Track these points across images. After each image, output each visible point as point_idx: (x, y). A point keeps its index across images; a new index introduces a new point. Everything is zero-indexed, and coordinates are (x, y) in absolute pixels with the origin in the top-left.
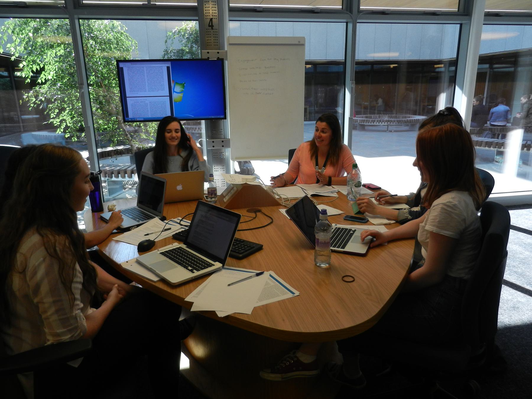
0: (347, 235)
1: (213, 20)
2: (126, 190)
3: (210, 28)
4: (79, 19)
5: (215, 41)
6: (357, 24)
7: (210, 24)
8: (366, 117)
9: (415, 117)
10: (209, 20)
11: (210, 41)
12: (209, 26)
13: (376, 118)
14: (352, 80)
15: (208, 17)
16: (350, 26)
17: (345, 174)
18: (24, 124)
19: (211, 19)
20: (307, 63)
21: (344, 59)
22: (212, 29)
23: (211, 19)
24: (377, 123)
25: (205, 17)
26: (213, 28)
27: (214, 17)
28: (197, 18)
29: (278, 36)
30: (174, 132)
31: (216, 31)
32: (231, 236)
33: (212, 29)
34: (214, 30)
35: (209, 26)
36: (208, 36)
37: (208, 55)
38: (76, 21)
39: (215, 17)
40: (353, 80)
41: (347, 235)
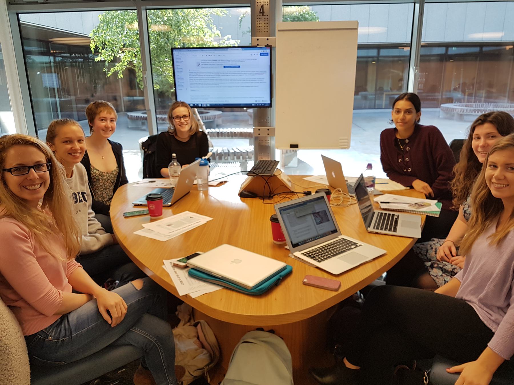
0: (384, 219)
1: (264, 6)
2: (164, 199)
3: (261, 14)
4: (146, 9)
5: (265, 28)
6: (425, 4)
7: (261, 11)
8: (466, 106)
9: (207, 113)
10: (260, 6)
11: (260, 28)
12: (260, 13)
13: (478, 106)
14: (416, 66)
15: (260, 4)
16: (417, 6)
17: (38, 73)
18: (216, 117)
19: (263, 6)
20: (361, 47)
21: (410, 41)
22: (263, 15)
23: (263, 6)
24: (469, 113)
25: (257, 4)
26: (264, 14)
27: (265, 4)
28: (249, 5)
29: (333, 20)
30: (109, 121)
31: (267, 17)
32: (291, 236)
33: (263, 15)
34: (265, 17)
35: (260, 13)
36: (258, 20)
37: (258, 42)
38: (143, 12)
39: (267, 4)
40: (417, 66)
41: (384, 219)
